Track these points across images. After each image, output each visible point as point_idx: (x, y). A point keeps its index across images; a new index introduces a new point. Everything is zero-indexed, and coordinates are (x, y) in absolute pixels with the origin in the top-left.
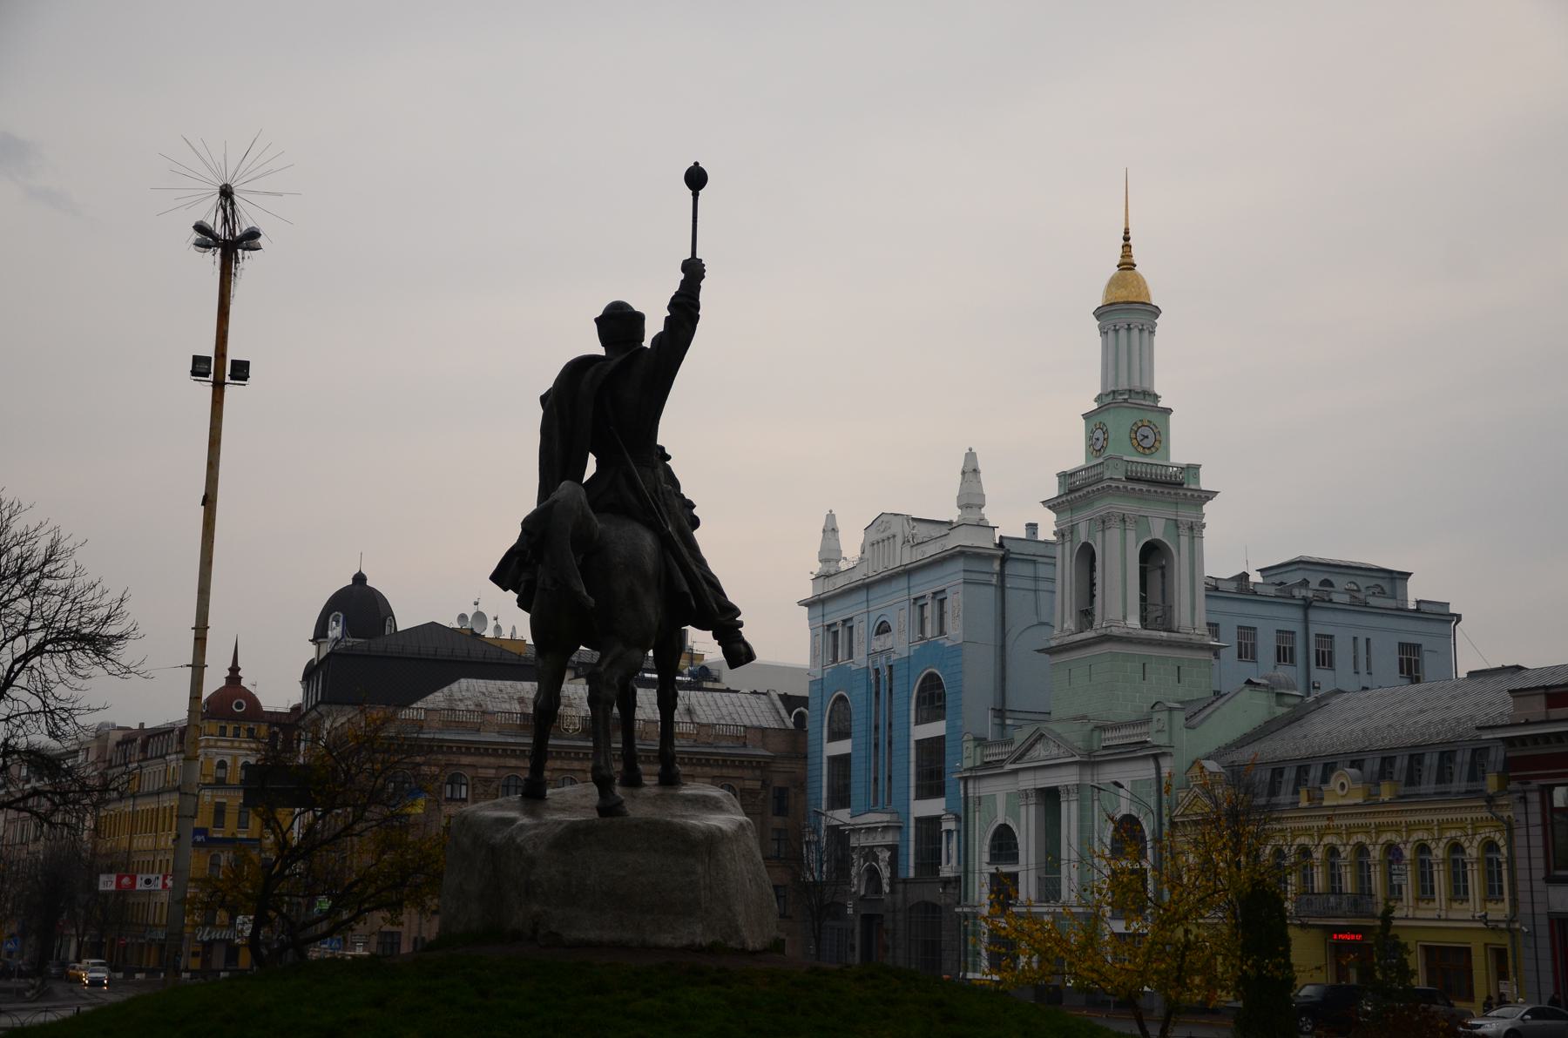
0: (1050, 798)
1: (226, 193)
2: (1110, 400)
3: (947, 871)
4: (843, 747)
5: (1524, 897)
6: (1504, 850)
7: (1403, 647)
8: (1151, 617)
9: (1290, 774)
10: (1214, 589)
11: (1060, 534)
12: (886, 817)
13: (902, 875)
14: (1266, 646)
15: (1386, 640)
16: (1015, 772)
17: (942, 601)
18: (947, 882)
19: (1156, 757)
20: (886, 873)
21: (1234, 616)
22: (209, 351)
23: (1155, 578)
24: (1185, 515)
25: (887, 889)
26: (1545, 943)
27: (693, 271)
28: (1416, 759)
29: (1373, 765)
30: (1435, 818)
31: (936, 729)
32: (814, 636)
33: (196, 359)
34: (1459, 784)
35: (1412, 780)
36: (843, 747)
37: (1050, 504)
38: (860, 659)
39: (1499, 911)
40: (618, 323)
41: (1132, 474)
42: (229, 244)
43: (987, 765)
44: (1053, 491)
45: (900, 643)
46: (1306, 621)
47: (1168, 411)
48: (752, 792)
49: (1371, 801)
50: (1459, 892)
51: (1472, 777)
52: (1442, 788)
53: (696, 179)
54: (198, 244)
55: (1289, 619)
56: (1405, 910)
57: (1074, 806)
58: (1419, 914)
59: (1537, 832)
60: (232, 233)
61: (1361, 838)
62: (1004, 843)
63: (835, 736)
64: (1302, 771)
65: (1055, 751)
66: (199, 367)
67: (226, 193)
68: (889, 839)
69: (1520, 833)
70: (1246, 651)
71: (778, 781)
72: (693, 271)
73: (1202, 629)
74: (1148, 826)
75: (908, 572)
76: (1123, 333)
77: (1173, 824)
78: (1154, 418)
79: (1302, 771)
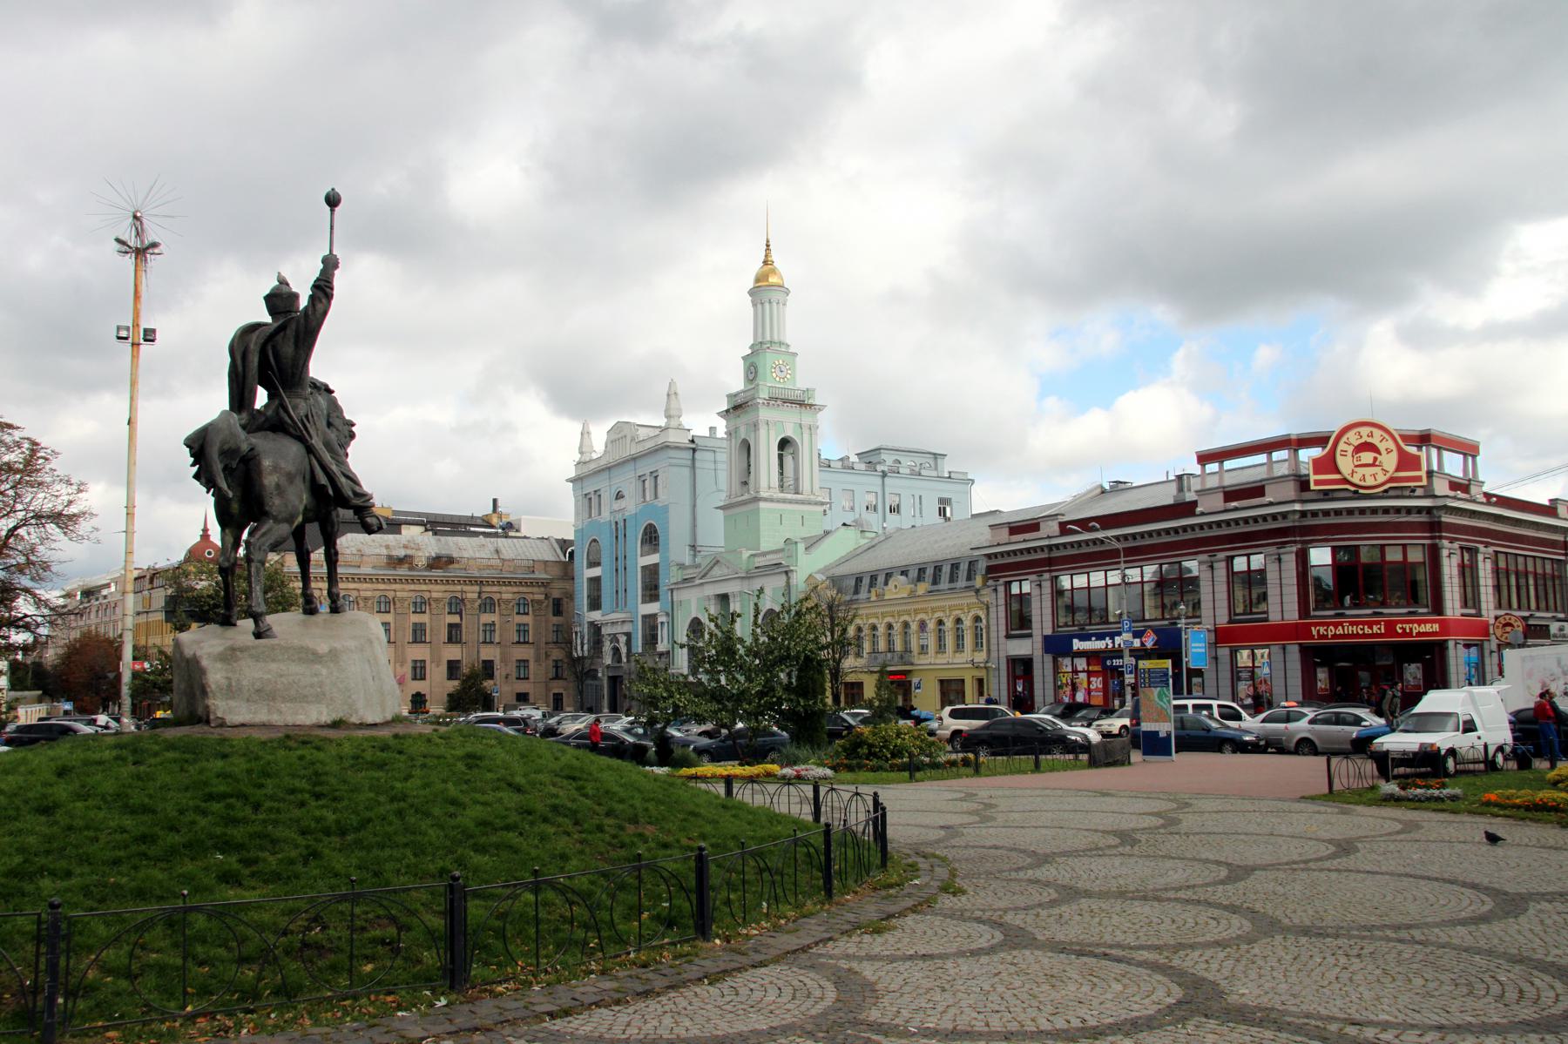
2: (758, 348)
5: (994, 648)
9: (866, 581)
10: (827, 465)
11: (729, 433)
18: (661, 655)
20: (624, 650)
21: (842, 480)
27: (330, 264)
28: (938, 569)
29: (913, 573)
37: (726, 414)
39: (981, 657)
48: (539, 602)
50: (959, 647)
51: (969, 578)
53: (333, 201)
56: (921, 661)
59: (1002, 609)
61: (906, 618)
69: (993, 610)
72: (330, 264)
75: (634, 459)
79: (874, 578)
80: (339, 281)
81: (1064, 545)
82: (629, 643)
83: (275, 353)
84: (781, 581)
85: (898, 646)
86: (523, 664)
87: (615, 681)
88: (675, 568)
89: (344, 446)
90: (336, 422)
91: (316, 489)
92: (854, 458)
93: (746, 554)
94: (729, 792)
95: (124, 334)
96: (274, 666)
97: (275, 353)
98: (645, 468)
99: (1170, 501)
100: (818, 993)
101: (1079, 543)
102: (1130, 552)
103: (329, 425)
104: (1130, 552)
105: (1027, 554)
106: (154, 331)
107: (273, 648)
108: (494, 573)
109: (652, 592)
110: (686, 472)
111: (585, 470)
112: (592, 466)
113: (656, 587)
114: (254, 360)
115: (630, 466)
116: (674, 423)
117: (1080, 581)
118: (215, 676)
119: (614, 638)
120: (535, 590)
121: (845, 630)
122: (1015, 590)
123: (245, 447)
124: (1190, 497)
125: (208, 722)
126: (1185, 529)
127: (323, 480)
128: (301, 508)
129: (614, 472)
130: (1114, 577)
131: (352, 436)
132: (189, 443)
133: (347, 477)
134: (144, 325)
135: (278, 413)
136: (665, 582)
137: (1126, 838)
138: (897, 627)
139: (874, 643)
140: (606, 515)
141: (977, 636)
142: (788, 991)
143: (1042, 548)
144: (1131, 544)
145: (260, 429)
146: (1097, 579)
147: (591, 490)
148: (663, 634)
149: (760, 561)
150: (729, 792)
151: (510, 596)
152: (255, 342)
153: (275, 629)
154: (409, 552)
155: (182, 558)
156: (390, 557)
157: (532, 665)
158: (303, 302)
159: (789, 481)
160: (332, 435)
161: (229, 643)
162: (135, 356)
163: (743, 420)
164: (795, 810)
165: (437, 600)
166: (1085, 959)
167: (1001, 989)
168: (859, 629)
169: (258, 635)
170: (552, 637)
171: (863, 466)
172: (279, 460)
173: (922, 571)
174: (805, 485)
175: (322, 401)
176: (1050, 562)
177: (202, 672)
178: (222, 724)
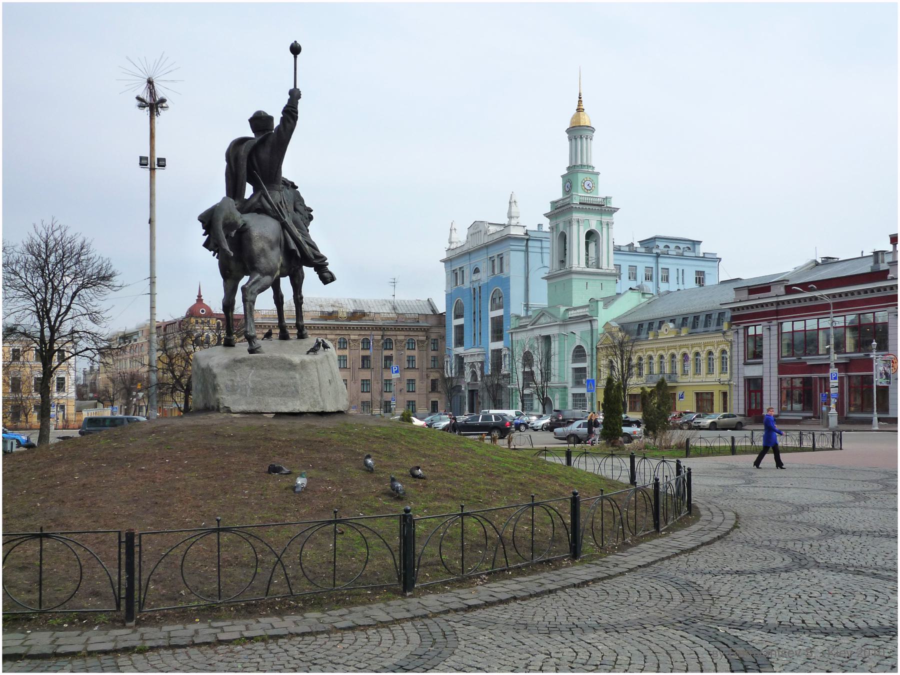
0: (547, 339)
1: (150, 82)
2: (573, 169)
3: (504, 371)
4: (460, 321)
5: (735, 371)
6: (729, 353)
7: (698, 272)
8: (590, 263)
9: (646, 326)
10: (618, 250)
11: (552, 228)
12: (479, 350)
13: (486, 373)
14: (641, 273)
15: (690, 269)
16: (532, 329)
17: (501, 258)
18: (504, 376)
19: (590, 321)
20: (479, 373)
21: (626, 262)
22: (147, 154)
23: (592, 246)
24: (605, 219)
25: (479, 379)
26: (742, 389)
27: (295, 95)
28: (696, 318)
29: (679, 321)
30: (702, 341)
31: (500, 312)
32: (447, 276)
33: (141, 158)
34: (713, 327)
35: (694, 326)
36: (460, 321)
37: (548, 216)
38: (467, 284)
39: (725, 377)
40: (259, 121)
41: (576, 203)
42: (153, 105)
43: (521, 327)
44: (548, 210)
45: (484, 276)
46: (657, 262)
47: (598, 174)
48: (422, 341)
49: (678, 335)
50: (710, 371)
51: (718, 324)
52: (706, 329)
53: (295, 50)
54: (140, 106)
55: (650, 262)
56: (681, 379)
57: (557, 342)
58: (695, 380)
59: (742, 345)
60: (154, 100)
61: (673, 351)
62: (528, 359)
63: (457, 316)
64: (651, 324)
65: (549, 320)
66: (143, 162)
67: (150, 82)
68: (480, 359)
69: (735, 346)
70: (633, 276)
71: (433, 336)
72: (295, 95)
73: (612, 267)
74: (587, 350)
75: (487, 246)
76: (579, 140)
77: (597, 348)
78: (592, 177)
79: (651, 324)
80: (302, 106)
81: (788, 301)
82: (482, 369)
83: (258, 156)
84: (586, 327)
85: (667, 370)
86: (411, 382)
87: (472, 393)
88: (513, 319)
89: (307, 225)
90: (300, 208)
91: (288, 253)
92: (637, 245)
93: (563, 309)
94: (569, 462)
95: (144, 162)
96: (263, 372)
97: (258, 156)
98: (494, 252)
99: (869, 270)
100: (668, 596)
101: (799, 300)
102: (837, 305)
103: (295, 210)
104: (837, 305)
105: (759, 305)
106: (164, 160)
107: (262, 359)
108: (392, 323)
109: (498, 334)
110: (522, 254)
111: (453, 253)
112: (458, 251)
113: (501, 331)
114: (244, 164)
115: (485, 251)
116: (514, 222)
117: (799, 326)
118: (223, 380)
119: (472, 365)
120: (421, 333)
121: (630, 359)
122: (751, 331)
123: (240, 223)
124: (883, 267)
125: (218, 410)
126: (879, 289)
127: (293, 246)
128: (279, 265)
129: (472, 256)
130: (825, 323)
131: (311, 218)
132: (202, 218)
133: (309, 245)
134: (158, 155)
135: (260, 200)
136: (507, 328)
137: (857, 496)
138: (667, 358)
139: (651, 368)
140: (467, 284)
141: (723, 361)
142: (645, 594)
143: (772, 304)
144: (836, 300)
145: (248, 211)
146: (812, 324)
147: (458, 267)
148: (506, 361)
149: (572, 314)
150: (569, 462)
151: (402, 338)
152: (244, 151)
153: (263, 348)
154: (335, 309)
155: (184, 315)
156: (322, 312)
157: (417, 383)
158: (277, 123)
159: (592, 260)
160: (298, 217)
161: (232, 357)
162: (152, 177)
163: (561, 221)
164: (617, 473)
165: (354, 340)
166: (860, 577)
167: (805, 597)
168: (640, 359)
169: (251, 351)
170: (431, 365)
171: (643, 250)
172: (263, 229)
173: (685, 319)
174: (604, 265)
175: (289, 192)
176: (777, 313)
177: (215, 376)
178: (228, 411)
